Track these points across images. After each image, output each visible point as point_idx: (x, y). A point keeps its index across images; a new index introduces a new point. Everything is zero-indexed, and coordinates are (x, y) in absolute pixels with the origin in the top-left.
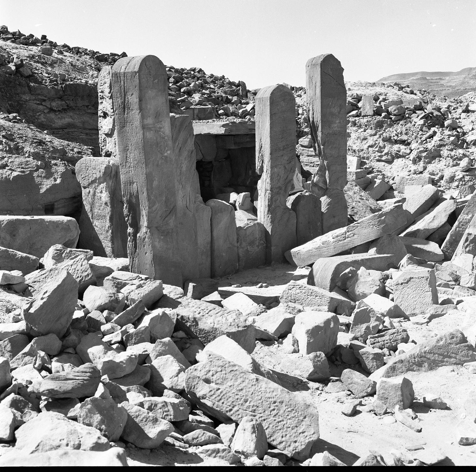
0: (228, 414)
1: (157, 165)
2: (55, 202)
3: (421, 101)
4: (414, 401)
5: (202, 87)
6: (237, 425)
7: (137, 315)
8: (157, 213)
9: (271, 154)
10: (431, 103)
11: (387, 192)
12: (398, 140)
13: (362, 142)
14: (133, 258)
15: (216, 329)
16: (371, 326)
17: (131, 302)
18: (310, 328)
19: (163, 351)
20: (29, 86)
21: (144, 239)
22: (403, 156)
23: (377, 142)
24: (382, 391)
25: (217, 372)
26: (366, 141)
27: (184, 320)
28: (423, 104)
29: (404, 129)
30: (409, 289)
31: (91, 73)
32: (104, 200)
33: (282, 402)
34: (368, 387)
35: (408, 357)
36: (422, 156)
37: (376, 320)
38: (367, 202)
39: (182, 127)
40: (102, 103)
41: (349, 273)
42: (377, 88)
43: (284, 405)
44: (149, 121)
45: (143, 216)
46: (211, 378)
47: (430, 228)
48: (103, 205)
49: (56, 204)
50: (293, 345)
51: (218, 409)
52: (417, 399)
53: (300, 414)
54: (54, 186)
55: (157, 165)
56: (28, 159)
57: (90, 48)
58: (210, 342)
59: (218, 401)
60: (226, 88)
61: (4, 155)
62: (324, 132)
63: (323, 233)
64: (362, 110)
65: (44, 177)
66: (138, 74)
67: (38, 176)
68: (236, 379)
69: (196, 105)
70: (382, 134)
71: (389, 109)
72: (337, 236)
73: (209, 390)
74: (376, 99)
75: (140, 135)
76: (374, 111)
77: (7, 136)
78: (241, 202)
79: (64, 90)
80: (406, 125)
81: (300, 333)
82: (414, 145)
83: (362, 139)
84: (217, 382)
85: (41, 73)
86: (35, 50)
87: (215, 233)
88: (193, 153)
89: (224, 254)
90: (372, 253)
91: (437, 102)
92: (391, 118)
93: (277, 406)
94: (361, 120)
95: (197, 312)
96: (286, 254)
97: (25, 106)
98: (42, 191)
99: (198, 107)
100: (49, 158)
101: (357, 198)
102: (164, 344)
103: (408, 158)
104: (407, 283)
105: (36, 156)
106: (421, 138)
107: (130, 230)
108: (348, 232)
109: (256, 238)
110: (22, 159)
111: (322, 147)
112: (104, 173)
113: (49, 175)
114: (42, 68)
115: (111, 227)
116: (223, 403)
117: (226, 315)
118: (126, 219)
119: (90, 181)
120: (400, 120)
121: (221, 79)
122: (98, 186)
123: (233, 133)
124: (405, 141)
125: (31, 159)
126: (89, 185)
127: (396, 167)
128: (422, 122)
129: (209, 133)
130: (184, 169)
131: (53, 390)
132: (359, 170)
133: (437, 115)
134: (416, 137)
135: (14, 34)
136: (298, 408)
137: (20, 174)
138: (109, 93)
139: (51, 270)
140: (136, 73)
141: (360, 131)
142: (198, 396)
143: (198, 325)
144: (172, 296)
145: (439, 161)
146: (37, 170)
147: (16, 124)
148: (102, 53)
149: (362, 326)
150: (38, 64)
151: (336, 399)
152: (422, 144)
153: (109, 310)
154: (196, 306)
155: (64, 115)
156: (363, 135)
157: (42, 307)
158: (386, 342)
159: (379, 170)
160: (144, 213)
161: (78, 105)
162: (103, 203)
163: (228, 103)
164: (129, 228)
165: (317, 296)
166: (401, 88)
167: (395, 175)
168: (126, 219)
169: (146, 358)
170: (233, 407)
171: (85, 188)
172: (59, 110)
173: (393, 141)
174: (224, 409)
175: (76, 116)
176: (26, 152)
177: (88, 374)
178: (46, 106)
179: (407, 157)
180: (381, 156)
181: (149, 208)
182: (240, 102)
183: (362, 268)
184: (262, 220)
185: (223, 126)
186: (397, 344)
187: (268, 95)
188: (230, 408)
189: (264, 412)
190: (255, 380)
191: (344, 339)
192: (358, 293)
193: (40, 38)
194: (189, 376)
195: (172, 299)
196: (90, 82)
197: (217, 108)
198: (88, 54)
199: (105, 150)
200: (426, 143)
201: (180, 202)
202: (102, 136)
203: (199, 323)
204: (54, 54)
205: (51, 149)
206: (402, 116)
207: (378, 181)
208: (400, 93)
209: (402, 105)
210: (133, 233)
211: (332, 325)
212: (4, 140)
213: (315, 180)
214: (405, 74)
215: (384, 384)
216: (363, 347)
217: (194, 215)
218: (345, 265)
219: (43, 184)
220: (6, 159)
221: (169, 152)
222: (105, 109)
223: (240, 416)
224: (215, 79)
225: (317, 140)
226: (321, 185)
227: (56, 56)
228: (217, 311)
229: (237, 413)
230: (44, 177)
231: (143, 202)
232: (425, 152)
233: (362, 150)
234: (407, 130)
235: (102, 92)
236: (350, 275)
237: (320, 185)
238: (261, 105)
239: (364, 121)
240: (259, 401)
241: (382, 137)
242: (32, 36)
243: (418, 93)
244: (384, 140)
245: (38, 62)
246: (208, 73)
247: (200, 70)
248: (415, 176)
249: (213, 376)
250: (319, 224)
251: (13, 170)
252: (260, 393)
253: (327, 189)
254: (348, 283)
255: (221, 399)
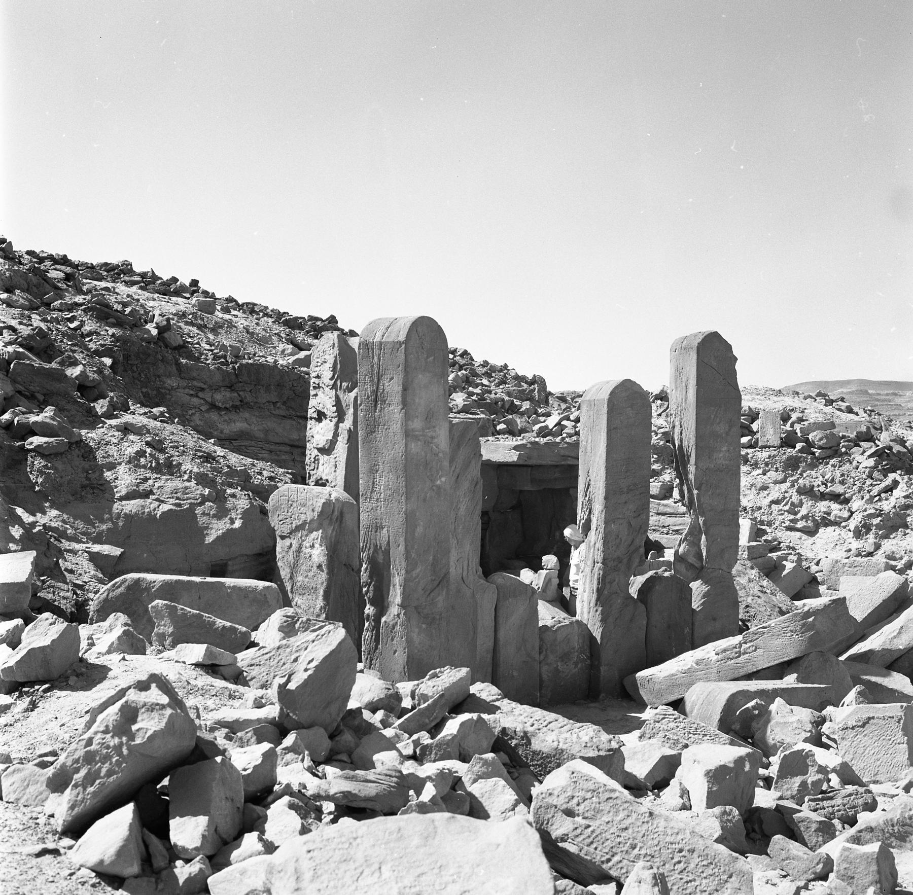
0: (604, 866)
1: (424, 500)
2: (230, 560)
3: (869, 425)
4: (897, 889)
5: (468, 381)
6: (620, 886)
7: (435, 718)
8: (419, 582)
9: (606, 498)
10: (887, 430)
11: (806, 585)
12: (827, 494)
13: (758, 494)
14: (371, 661)
15: (562, 750)
16: (809, 781)
17: (419, 700)
18: (712, 767)
19: (484, 773)
20: (178, 364)
21: (394, 626)
22: (836, 523)
23: (786, 495)
24: (845, 865)
25: (585, 800)
26: (766, 492)
27: (507, 735)
28: (873, 431)
29: (838, 474)
30: (866, 738)
31: (281, 347)
32: (316, 560)
33: (692, 851)
34: (818, 864)
35: (881, 822)
36: (872, 525)
37: (818, 772)
38: (774, 598)
39: (466, 438)
40: (316, 395)
41: (754, 708)
42: (786, 399)
43: (695, 855)
44: (417, 424)
45: (394, 586)
46: (577, 808)
47: (894, 647)
48: (315, 569)
49: (230, 563)
50: (682, 797)
51: (588, 858)
52: (901, 886)
53: (722, 870)
54: (229, 534)
55: (424, 500)
56: (187, 484)
57: (273, 305)
58: (549, 772)
59: (588, 845)
60: (510, 387)
61: (148, 475)
62: (700, 465)
63: (694, 647)
64: (758, 435)
65: (214, 516)
66: (403, 346)
67: (203, 514)
68: (617, 812)
69: (458, 412)
70: (797, 481)
71: (810, 437)
72: (724, 651)
73: (572, 827)
74: (785, 418)
75: (400, 447)
76: (781, 439)
77: (154, 444)
78: (541, 586)
79: (238, 374)
80: (840, 466)
81: (692, 778)
82: (856, 504)
83: (758, 487)
84: (586, 815)
85: (198, 343)
86: (181, 304)
87: (502, 634)
88: (478, 486)
89: (515, 674)
90: (790, 681)
91: (898, 430)
92: (814, 453)
93: (685, 857)
94: (757, 453)
95: (529, 724)
96: (627, 682)
97: (168, 397)
98: (209, 539)
99: (462, 415)
100: (222, 484)
101: (756, 590)
102: (486, 763)
103: (845, 527)
104: (863, 726)
105: (202, 479)
106: (869, 492)
107: (369, 610)
108: (746, 643)
109: (574, 648)
110: (178, 483)
111: (695, 492)
112: (321, 514)
113: (222, 512)
114: (198, 334)
115: (325, 608)
116: (596, 849)
117: (577, 730)
118: (365, 589)
119: (294, 525)
120: (830, 457)
121: (501, 371)
122: (307, 536)
123: (530, 463)
124: (839, 495)
125: (193, 483)
126: (290, 533)
127: (823, 541)
128: (871, 462)
129: (489, 460)
130: (462, 511)
131: (349, 792)
132: (754, 544)
133: (899, 452)
134: (861, 489)
135: (143, 275)
136: (719, 861)
137: (174, 508)
138: (331, 379)
139: (279, 648)
140: (400, 343)
141: (755, 473)
142: (553, 837)
143: (530, 744)
144: (484, 696)
145: (905, 535)
146: (202, 503)
147: (165, 425)
148: (295, 315)
149: (793, 780)
150: (191, 328)
151: (765, 880)
152: (871, 503)
153: (385, 710)
154: (526, 714)
155: (233, 416)
156: (761, 480)
157: (306, 683)
158: (836, 808)
159: (791, 545)
160: (397, 580)
161: (260, 400)
162: (315, 566)
163: (513, 413)
164: (368, 606)
165: (706, 735)
166: (829, 402)
167: (821, 555)
168: (365, 589)
169: (456, 784)
170: (613, 856)
171: (283, 538)
172: (226, 408)
173: (818, 493)
174: (598, 857)
175: (254, 419)
176: (185, 472)
177: (395, 779)
178: (204, 400)
179: (843, 524)
180: (794, 521)
181: (407, 571)
182: (536, 413)
183: (779, 700)
184: (586, 616)
185: (516, 448)
186: (856, 813)
187: (605, 395)
188: (608, 856)
189: (664, 865)
190: (647, 815)
191: (764, 799)
192: (773, 742)
193: (188, 285)
194: (539, 804)
195: (485, 701)
196: (281, 362)
197: (494, 420)
198: (270, 316)
199: (315, 477)
200: (880, 500)
201: (454, 572)
202: (311, 452)
203: (533, 741)
204: (217, 313)
205: (226, 469)
206: (834, 450)
207: (789, 566)
208: (829, 409)
209: (835, 431)
210: (374, 615)
211: (747, 768)
212: (149, 450)
213: (681, 550)
214: (826, 382)
215: (847, 853)
216: (800, 811)
217: (473, 595)
218: (747, 695)
219: (212, 528)
220: (150, 482)
221: (443, 479)
222: (321, 406)
223: (624, 871)
224: (490, 370)
225: (687, 480)
226: (692, 560)
227: (220, 315)
228: (562, 724)
229: (620, 865)
230: (214, 516)
231: (397, 562)
232: (878, 516)
233: (760, 508)
234: (843, 475)
235: (318, 377)
236: (757, 712)
237: (690, 561)
238: (592, 413)
239: (764, 455)
240: (656, 848)
241: (796, 487)
242: (175, 280)
243: (861, 412)
244: (800, 492)
245: (192, 324)
246: (478, 359)
247: (465, 353)
248: (859, 559)
249: (578, 805)
250: (687, 630)
251: (162, 502)
252: (656, 835)
253: (702, 567)
254: (754, 724)
255: (592, 843)
